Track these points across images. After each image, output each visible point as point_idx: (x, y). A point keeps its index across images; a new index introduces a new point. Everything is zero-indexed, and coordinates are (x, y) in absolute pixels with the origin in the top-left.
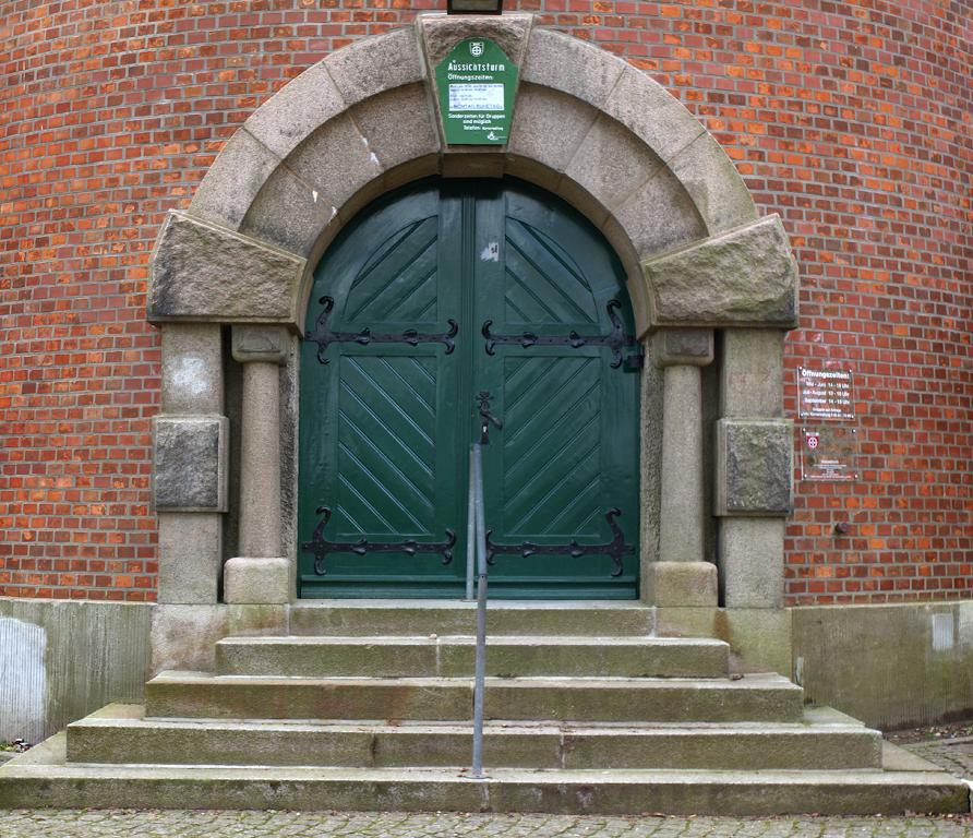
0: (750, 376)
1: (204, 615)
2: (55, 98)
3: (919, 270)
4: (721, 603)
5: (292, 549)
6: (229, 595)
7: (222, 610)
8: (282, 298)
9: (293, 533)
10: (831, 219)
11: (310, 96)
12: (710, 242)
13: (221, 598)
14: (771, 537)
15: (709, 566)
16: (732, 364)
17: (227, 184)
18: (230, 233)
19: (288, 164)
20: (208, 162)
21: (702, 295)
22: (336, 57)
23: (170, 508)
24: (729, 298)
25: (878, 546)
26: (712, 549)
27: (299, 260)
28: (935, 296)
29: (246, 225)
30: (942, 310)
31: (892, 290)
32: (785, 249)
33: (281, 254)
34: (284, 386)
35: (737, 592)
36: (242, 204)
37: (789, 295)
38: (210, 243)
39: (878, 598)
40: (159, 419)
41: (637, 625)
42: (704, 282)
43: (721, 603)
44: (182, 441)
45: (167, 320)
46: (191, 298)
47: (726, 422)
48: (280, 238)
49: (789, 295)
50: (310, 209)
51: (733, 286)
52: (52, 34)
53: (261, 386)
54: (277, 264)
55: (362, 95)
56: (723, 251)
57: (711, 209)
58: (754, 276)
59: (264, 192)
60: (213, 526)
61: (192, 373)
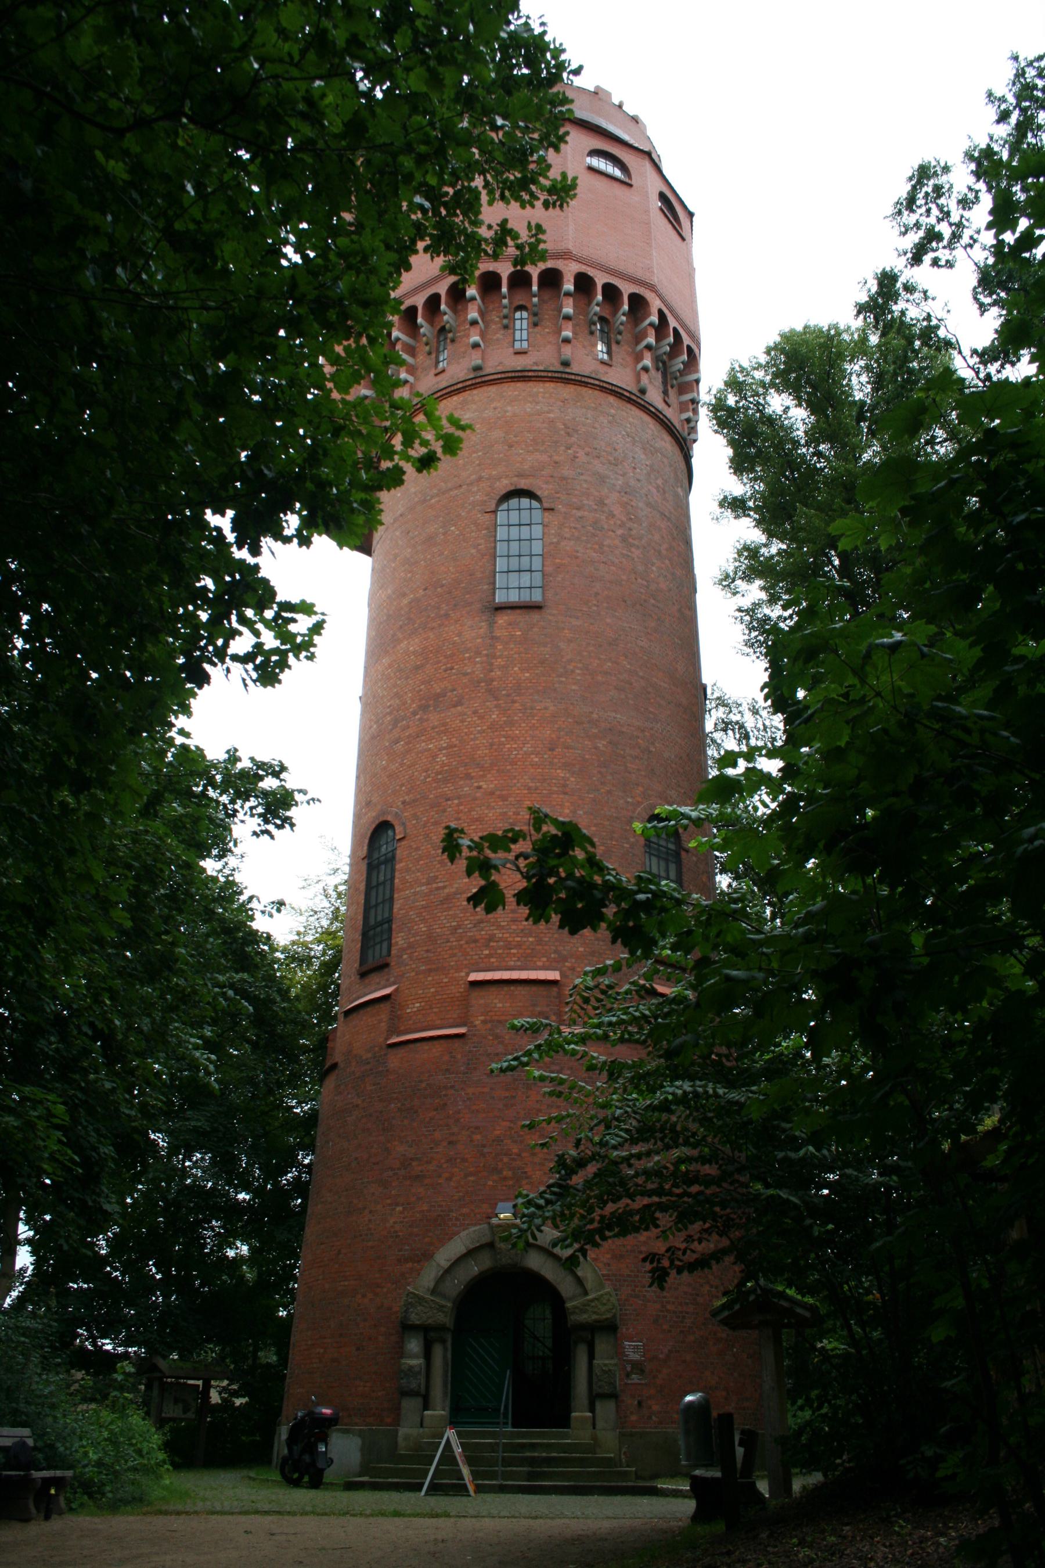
0: (602, 1345)
1: (415, 1432)
2: (370, 1244)
3: (673, 1303)
4: (594, 1428)
5: (448, 1409)
6: (425, 1425)
7: (421, 1430)
8: (445, 1319)
9: (448, 1402)
10: (636, 1286)
11: (456, 1247)
12: (589, 1297)
13: (422, 1426)
14: (611, 1405)
15: (590, 1414)
16: (597, 1341)
17: (428, 1278)
18: (428, 1296)
19: (448, 1271)
20: (421, 1269)
21: (585, 1316)
22: (463, 1234)
23: (406, 1393)
24: (594, 1317)
25: (656, 1408)
26: (592, 1410)
27: (449, 1305)
28: (681, 1312)
29: (433, 1292)
30: (684, 1317)
31: (662, 1311)
32: (613, 1299)
33: (443, 1302)
34: (445, 1349)
35: (600, 1424)
36: (432, 1285)
37: (614, 1316)
38: (420, 1299)
39: (656, 1428)
40: (403, 1361)
41: (566, 1436)
42: (585, 1312)
43: (594, 1428)
44: (411, 1367)
45: (407, 1328)
46: (414, 1319)
47: (595, 1362)
48: (444, 1296)
49: (614, 1316)
50: (455, 1286)
51: (595, 1313)
52: (370, 1221)
53: (438, 1351)
54: (443, 1306)
55: (472, 1247)
56: (592, 1300)
57: (589, 1285)
58: (603, 1309)
59: (440, 1280)
60: (420, 1400)
61: (414, 1345)
